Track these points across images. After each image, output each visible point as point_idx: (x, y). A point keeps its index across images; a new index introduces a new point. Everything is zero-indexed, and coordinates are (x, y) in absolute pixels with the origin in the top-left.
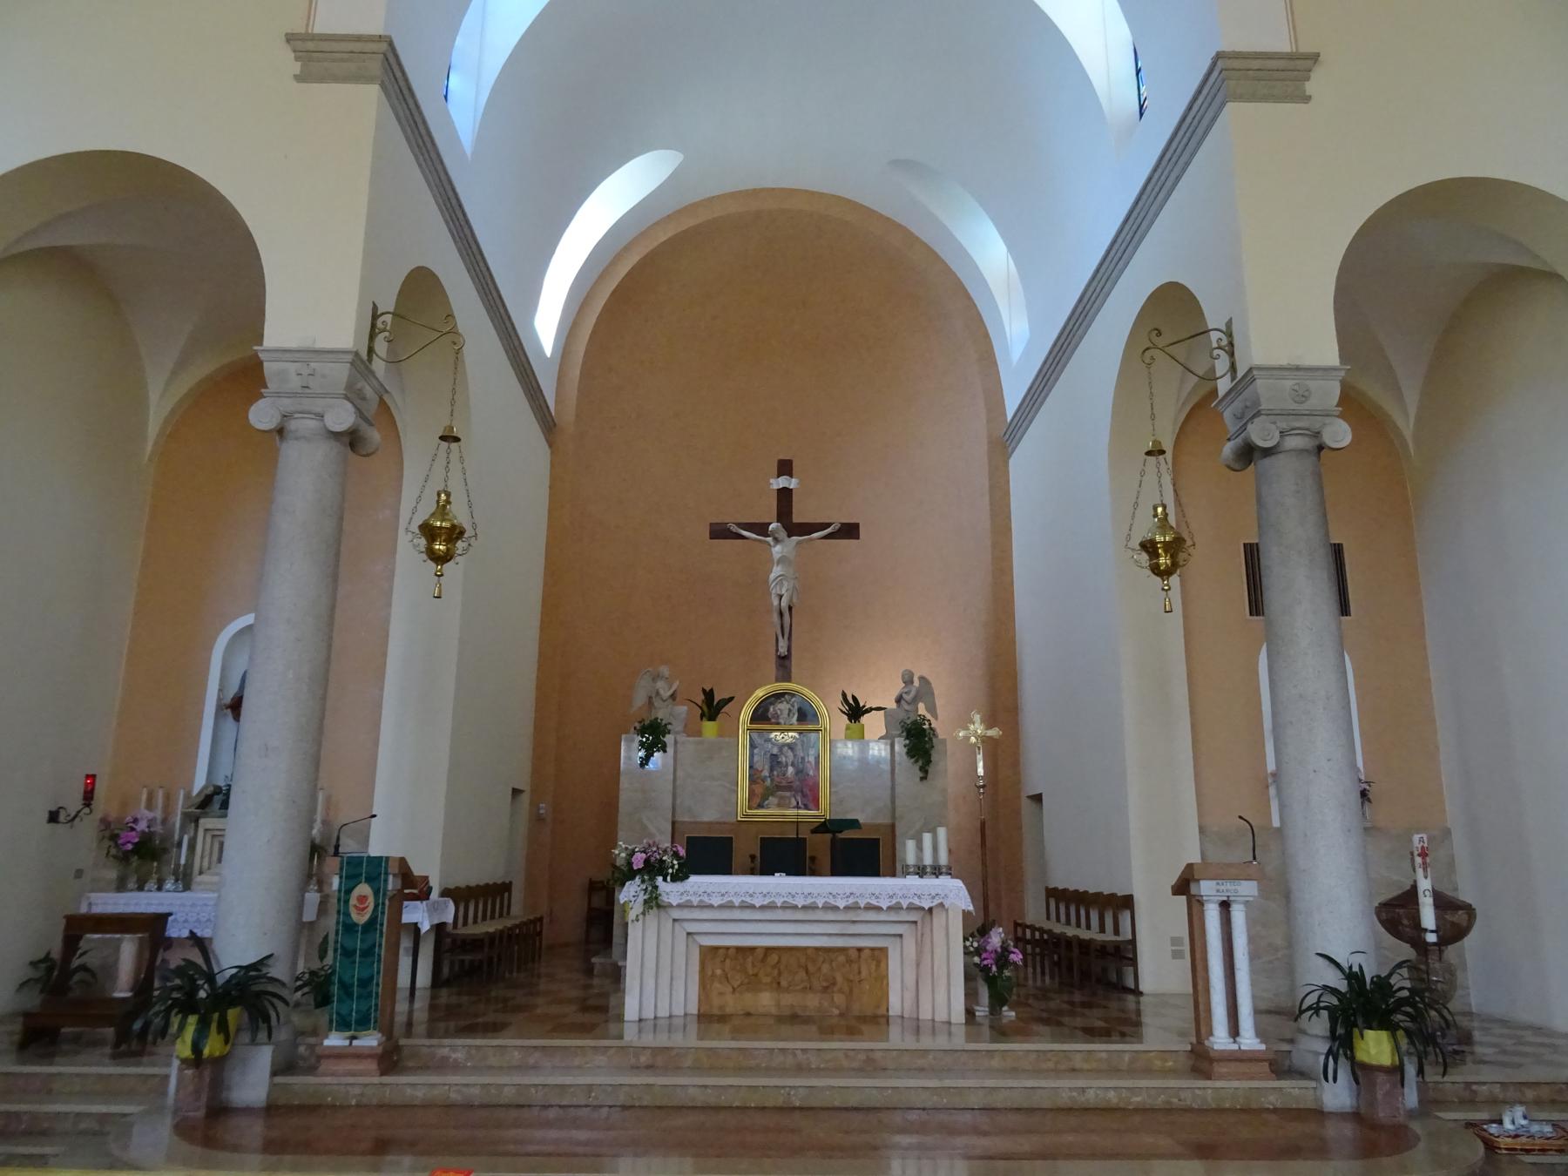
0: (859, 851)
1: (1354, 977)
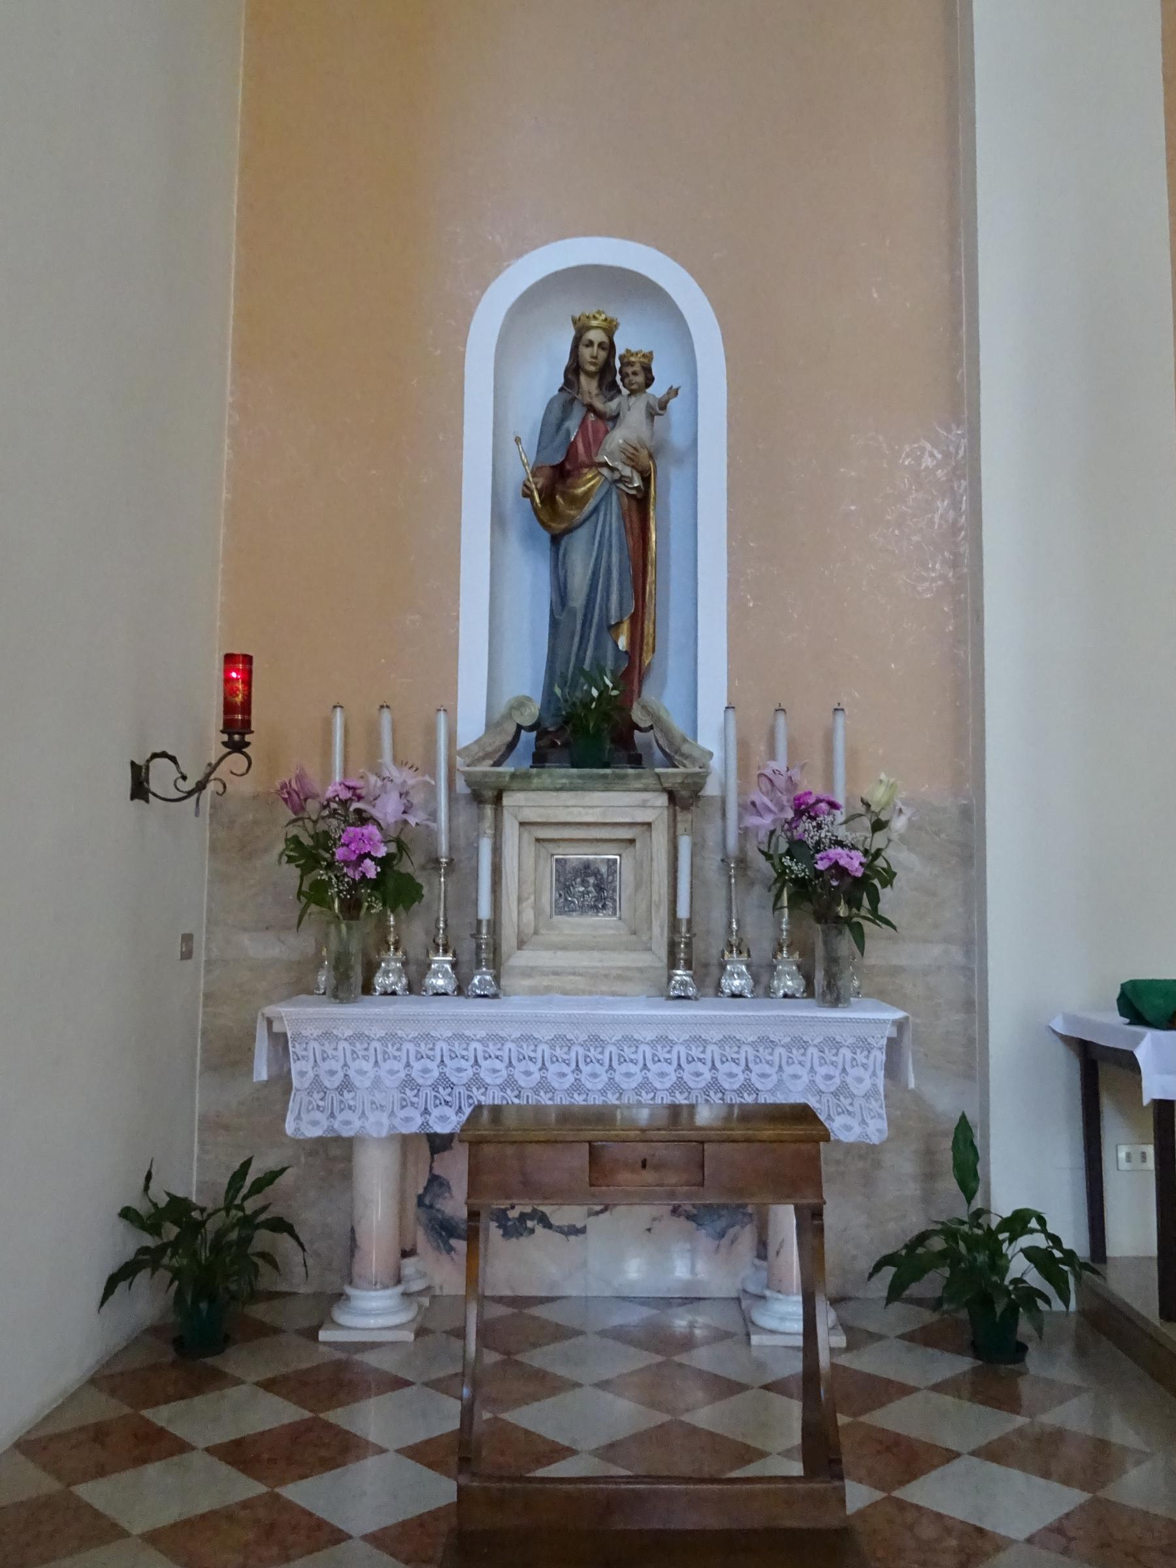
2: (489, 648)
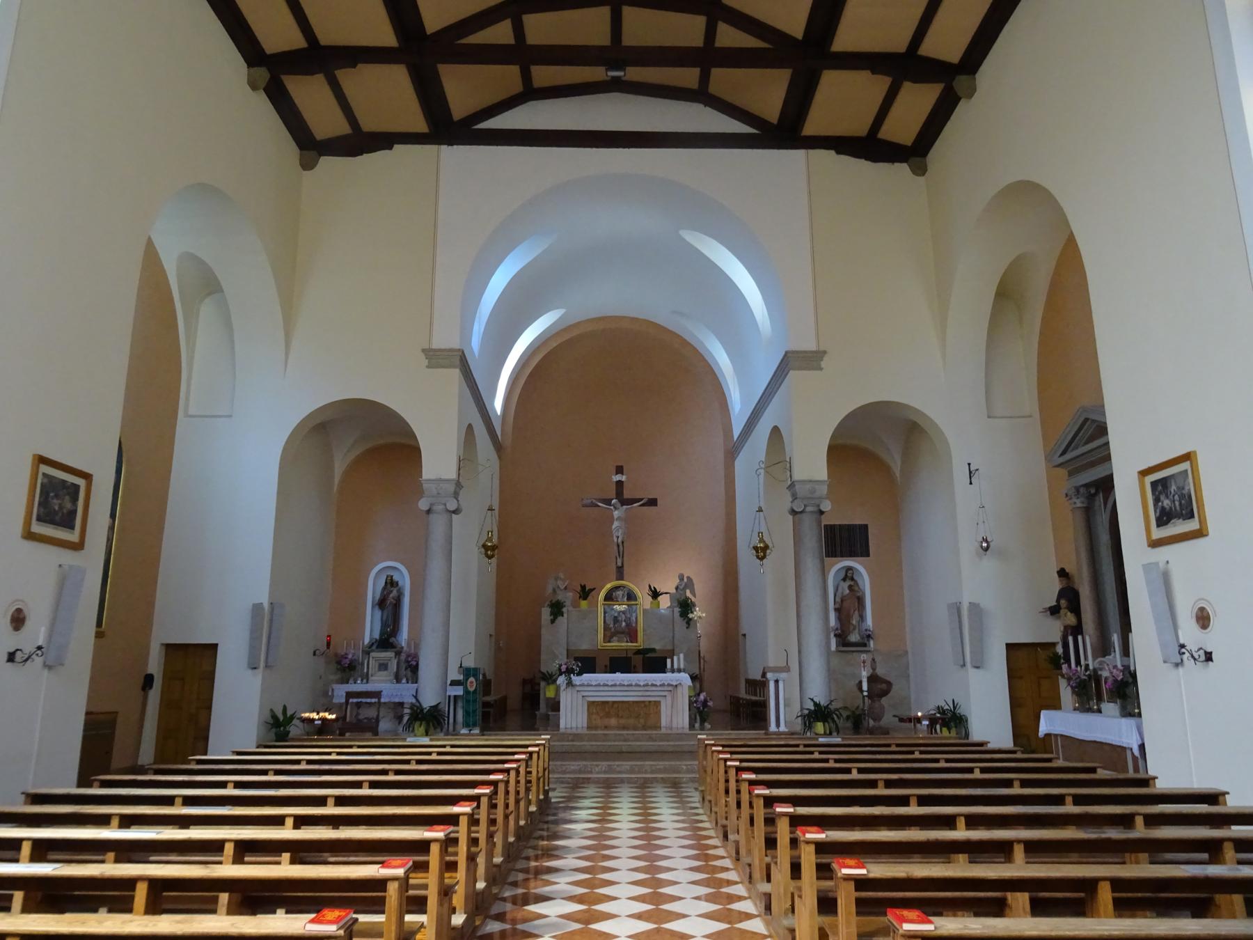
0: (654, 663)
1: (816, 704)
2: (371, 627)
